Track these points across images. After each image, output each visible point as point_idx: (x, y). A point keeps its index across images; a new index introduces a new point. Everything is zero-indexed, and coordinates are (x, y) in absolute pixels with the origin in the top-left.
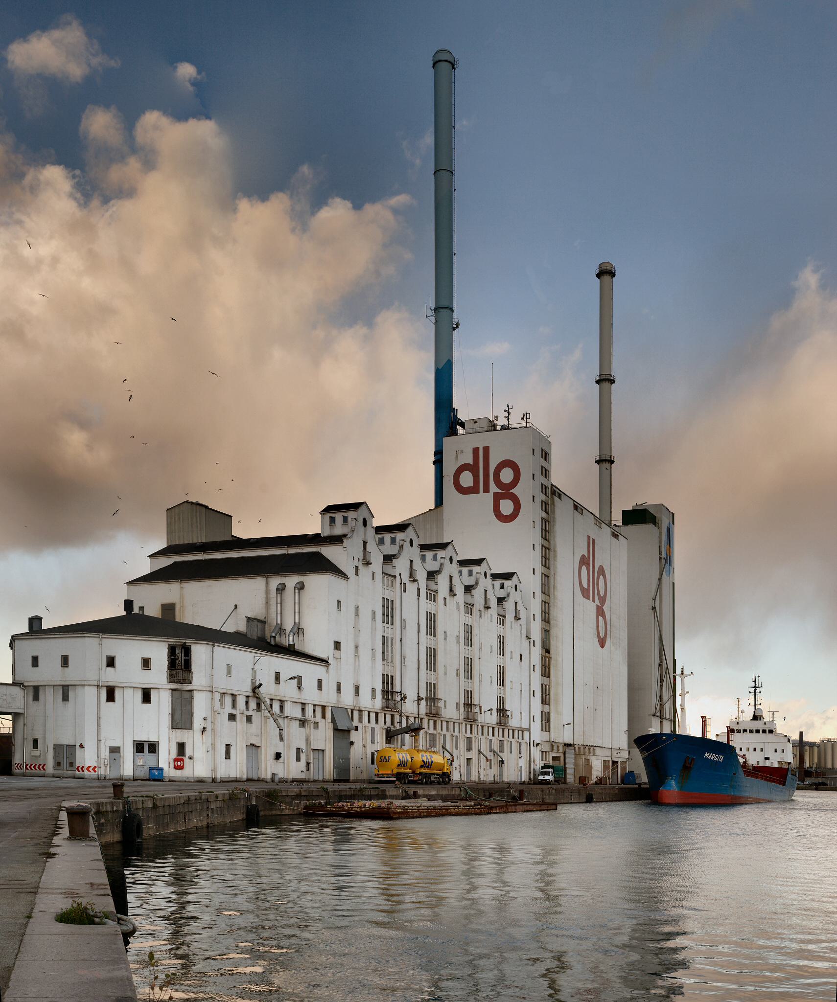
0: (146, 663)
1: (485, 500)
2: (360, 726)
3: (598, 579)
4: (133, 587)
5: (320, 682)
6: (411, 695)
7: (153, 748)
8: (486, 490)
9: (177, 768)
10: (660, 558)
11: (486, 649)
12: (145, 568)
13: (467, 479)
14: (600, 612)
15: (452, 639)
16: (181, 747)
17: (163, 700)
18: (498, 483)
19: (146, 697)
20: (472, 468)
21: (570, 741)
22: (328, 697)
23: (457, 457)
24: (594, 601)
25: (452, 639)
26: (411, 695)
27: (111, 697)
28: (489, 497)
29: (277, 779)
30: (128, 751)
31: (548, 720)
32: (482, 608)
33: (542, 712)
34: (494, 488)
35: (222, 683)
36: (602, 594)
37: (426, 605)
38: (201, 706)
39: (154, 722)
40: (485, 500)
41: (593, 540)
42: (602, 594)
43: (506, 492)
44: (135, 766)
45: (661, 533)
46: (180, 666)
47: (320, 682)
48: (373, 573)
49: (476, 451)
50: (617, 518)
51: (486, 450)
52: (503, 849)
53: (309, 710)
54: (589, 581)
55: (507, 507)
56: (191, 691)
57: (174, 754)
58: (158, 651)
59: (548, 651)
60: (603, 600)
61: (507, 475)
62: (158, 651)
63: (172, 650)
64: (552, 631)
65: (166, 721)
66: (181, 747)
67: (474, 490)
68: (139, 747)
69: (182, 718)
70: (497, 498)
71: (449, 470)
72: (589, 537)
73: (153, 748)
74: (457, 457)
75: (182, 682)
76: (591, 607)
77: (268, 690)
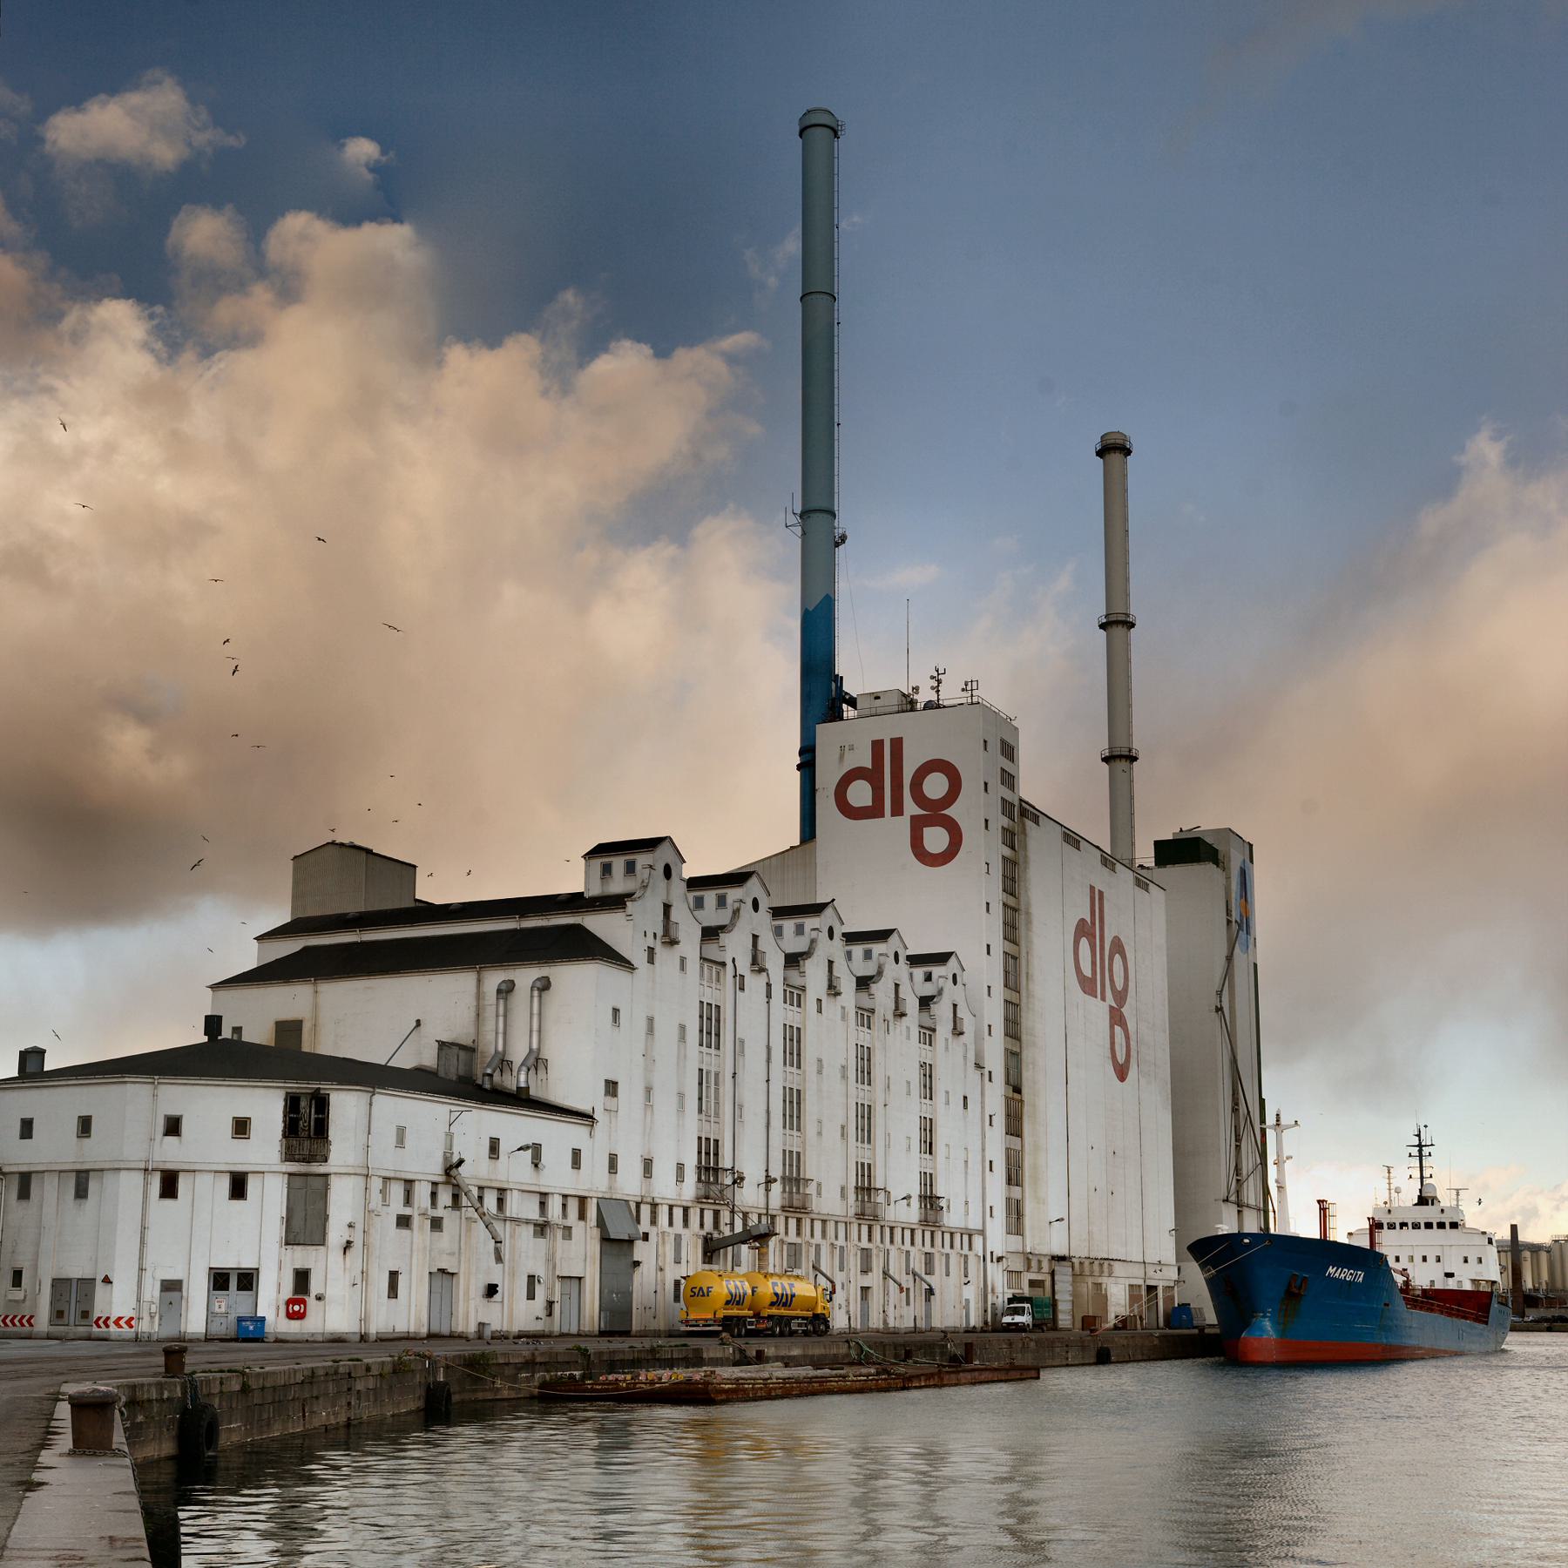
0: (241, 1127)
5: (576, 1154)
7: (247, 1280)
8: (898, 810)
9: (292, 1316)
10: (1229, 922)
12: (249, 958)
13: (860, 794)
14: (1117, 1018)
16: (302, 1278)
17: (270, 1194)
18: (919, 798)
19: (238, 1187)
20: (872, 775)
21: (1063, 1252)
22: (593, 1180)
23: (842, 757)
24: (1103, 999)
26: (753, 1172)
28: (903, 825)
29: (487, 1333)
30: (197, 1289)
31: (1019, 1215)
32: (890, 1017)
33: (1008, 1200)
34: (911, 808)
35: (387, 1159)
36: (1119, 985)
37: (782, 1014)
39: (253, 1234)
41: (1101, 893)
42: (1119, 985)
43: (935, 813)
45: (1228, 878)
46: (306, 1131)
47: (576, 1154)
48: (683, 960)
49: (877, 746)
51: (897, 744)
53: (555, 1205)
54: (1094, 963)
55: (936, 839)
56: (326, 1175)
57: (288, 1291)
58: (265, 1105)
59: (1017, 1090)
60: (1121, 997)
61: (936, 786)
62: (265, 1105)
63: (292, 1103)
66: (302, 1278)
67: (874, 811)
68: (220, 1280)
69: (305, 1222)
70: (917, 825)
71: (827, 778)
72: (1092, 888)
73: (247, 1280)
74: (842, 757)
76: (1099, 1009)
77: (476, 1169)
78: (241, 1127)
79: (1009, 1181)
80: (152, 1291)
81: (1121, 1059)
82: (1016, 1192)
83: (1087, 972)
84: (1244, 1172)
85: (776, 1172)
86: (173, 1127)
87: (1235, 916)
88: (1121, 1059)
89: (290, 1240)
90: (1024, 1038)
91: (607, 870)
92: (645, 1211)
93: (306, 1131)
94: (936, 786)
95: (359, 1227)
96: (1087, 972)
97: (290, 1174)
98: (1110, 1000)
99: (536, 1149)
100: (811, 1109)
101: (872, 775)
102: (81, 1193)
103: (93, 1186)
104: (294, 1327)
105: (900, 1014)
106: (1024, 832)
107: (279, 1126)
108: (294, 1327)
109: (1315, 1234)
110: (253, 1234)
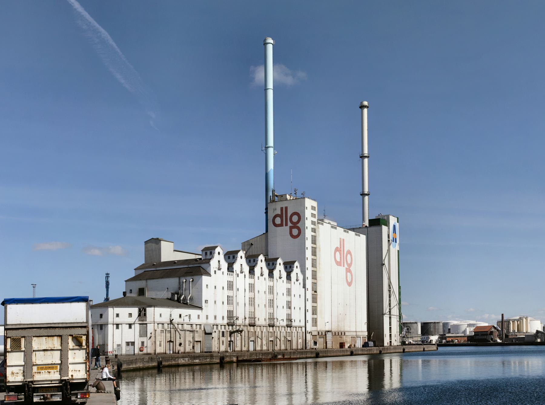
0: (130, 315)
1: (286, 229)
2: (217, 331)
3: (346, 256)
4: (127, 282)
5: (199, 316)
6: (241, 317)
7: (133, 343)
8: (286, 225)
9: (141, 351)
10: (389, 241)
11: (280, 294)
12: (133, 275)
13: (278, 221)
14: (348, 270)
15: (262, 293)
16: (143, 343)
17: (137, 327)
18: (291, 221)
19: (130, 326)
20: (281, 216)
21: (330, 329)
22: (203, 321)
24: (344, 266)
25: (262, 293)
26: (241, 317)
27: (117, 328)
28: (288, 228)
29: (180, 352)
30: (124, 345)
31: (316, 322)
32: (278, 278)
33: (313, 318)
34: (289, 224)
35: (158, 319)
36: (349, 262)
37: (249, 280)
38: (150, 328)
39: (133, 335)
40: (286, 229)
42: (349, 262)
43: (295, 225)
44: (126, 351)
45: (389, 228)
46: (142, 314)
47: (199, 316)
48: (223, 272)
49: (282, 209)
50: (367, 223)
51: (286, 208)
52: (528, 362)
53: (194, 326)
54: (341, 258)
55: (295, 232)
56: (146, 324)
57: (140, 346)
58: (135, 311)
59: (316, 292)
60: (350, 265)
62: (135, 311)
63: (140, 311)
64: (318, 284)
65: (137, 333)
66: (143, 343)
67: (281, 225)
68: (128, 344)
69: (143, 333)
70: (291, 228)
71: (271, 215)
72: (340, 239)
73: (133, 343)
75: (143, 321)
76: (342, 269)
77: (176, 320)
78: (130, 315)
79: (313, 314)
80: (115, 347)
81: (349, 280)
82: (315, 316)
83: (349, 256)
84: (392, 307)
85: (247, 316)
86: (118, 315)
87: (391, 238)
88: (349, 280)
89: (141, 336)
90: (318, 279)
91: (206, 254)
92: (215, 327)
93: (142, 314)
94: (295, 218)
95: (153, 334)
97: (140, 324)
98: (346, 266)
99: (190, 316)
100: (257, 302)
101: (281, 216)
102: (101, 329)
103: (103, 327)
104: (141, 352)
105: (280, 278)
106: (318, 228)
107: (137, 315)
108: (315, 347)
109: (8, 365)
110: (133, 335)
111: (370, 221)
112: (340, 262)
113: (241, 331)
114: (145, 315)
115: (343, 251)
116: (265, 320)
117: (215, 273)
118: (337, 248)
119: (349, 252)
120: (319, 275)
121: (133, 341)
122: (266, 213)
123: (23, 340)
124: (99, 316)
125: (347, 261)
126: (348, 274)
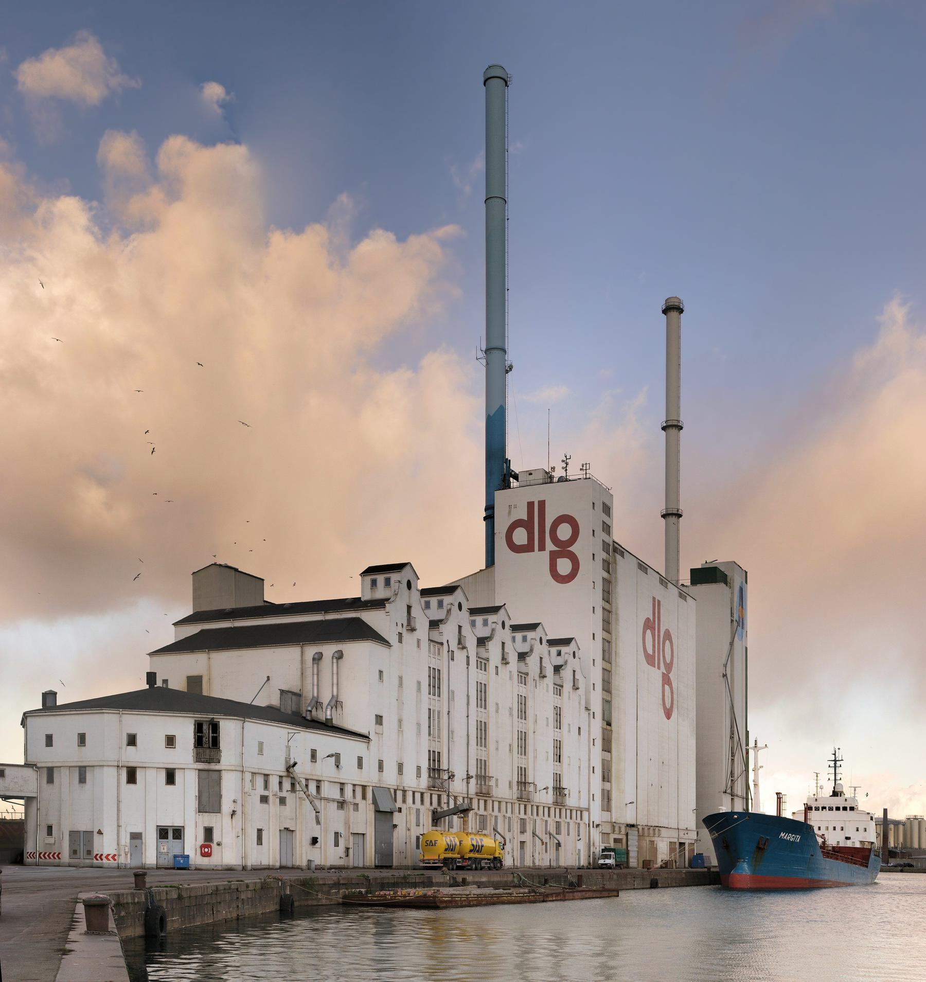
0: (170, 741)
1: (540, 559)
2: (404, 807)
5: (360, 760)
6: (460, 773)
7: (178, 833)
8: (542, 548)
9: (204, 855)
12: (170, 637)
13: (520, 536)
14: (666, 680)
15: (504, 711)
16: (209, 832)
17: (188, 781)
20: (527, 524)
22: (369, 776)
23: (510, 512)
24: (659, 668)
28: (545, 555)
30: (151, 837)
31: (609, 799)
32: (537, 678)
33: (603, 790)
34: (550, 546)
35: (254, 762)
36: (668, 661)
37: (476, 675)
38: (230, 787)
39: (179, 805)
40: (540, 559)
41: (659, 602)
42: (668, 661)
43: (564, 550)
46: (207, 742)
47: (360, 760)
48: (419, 640)
49: (530, 505)
50: (685, 578)
51: (542, 504)
53: (348, 790)
54: (654, 646)
55: (564, 566)
56: (220, 771)
57: (201, 840)
59: (609, 724)
60: (669, 667)
61: (564, 532)
62: (184, 728)
63: (199, 727)
64: (613, 702)
66: (209, 832)
67: (528, 548)
68: (163, 833)
69: (209, 801)
70: (554, 557)
71: (502, 525)
72: (654, 599)
73: (178, 833)
74: (510, 512)
75: (209, 761)
76: (656, 675)
78: (170, 741)
79: (604, 780)
80: (126, 839)
81: (668, 706)
83: (650, 652)
87: (736, 617)
88: (668, 706)
89: (201, 810)
91: (374, 583)
93: (207, 742)
94: (564, 532)
95: (239, 802)
96: (650, 652)
98: (663, 669)
99: (337, 757)
101: (527, 524)
111: (693, 571)
112: (653, 656)
113: (465, 811)
114: (215, 743)
115: (659, 631)
116: (510, 787)
117: (400, 641)
118: (648, 619)
119: (668, 636)
120: (616, 682)
121: (178, 823)
122: (490, 518)
123: (687, 865)
124: (75, 739)
125: (664, 656)
126: (667, 687)
